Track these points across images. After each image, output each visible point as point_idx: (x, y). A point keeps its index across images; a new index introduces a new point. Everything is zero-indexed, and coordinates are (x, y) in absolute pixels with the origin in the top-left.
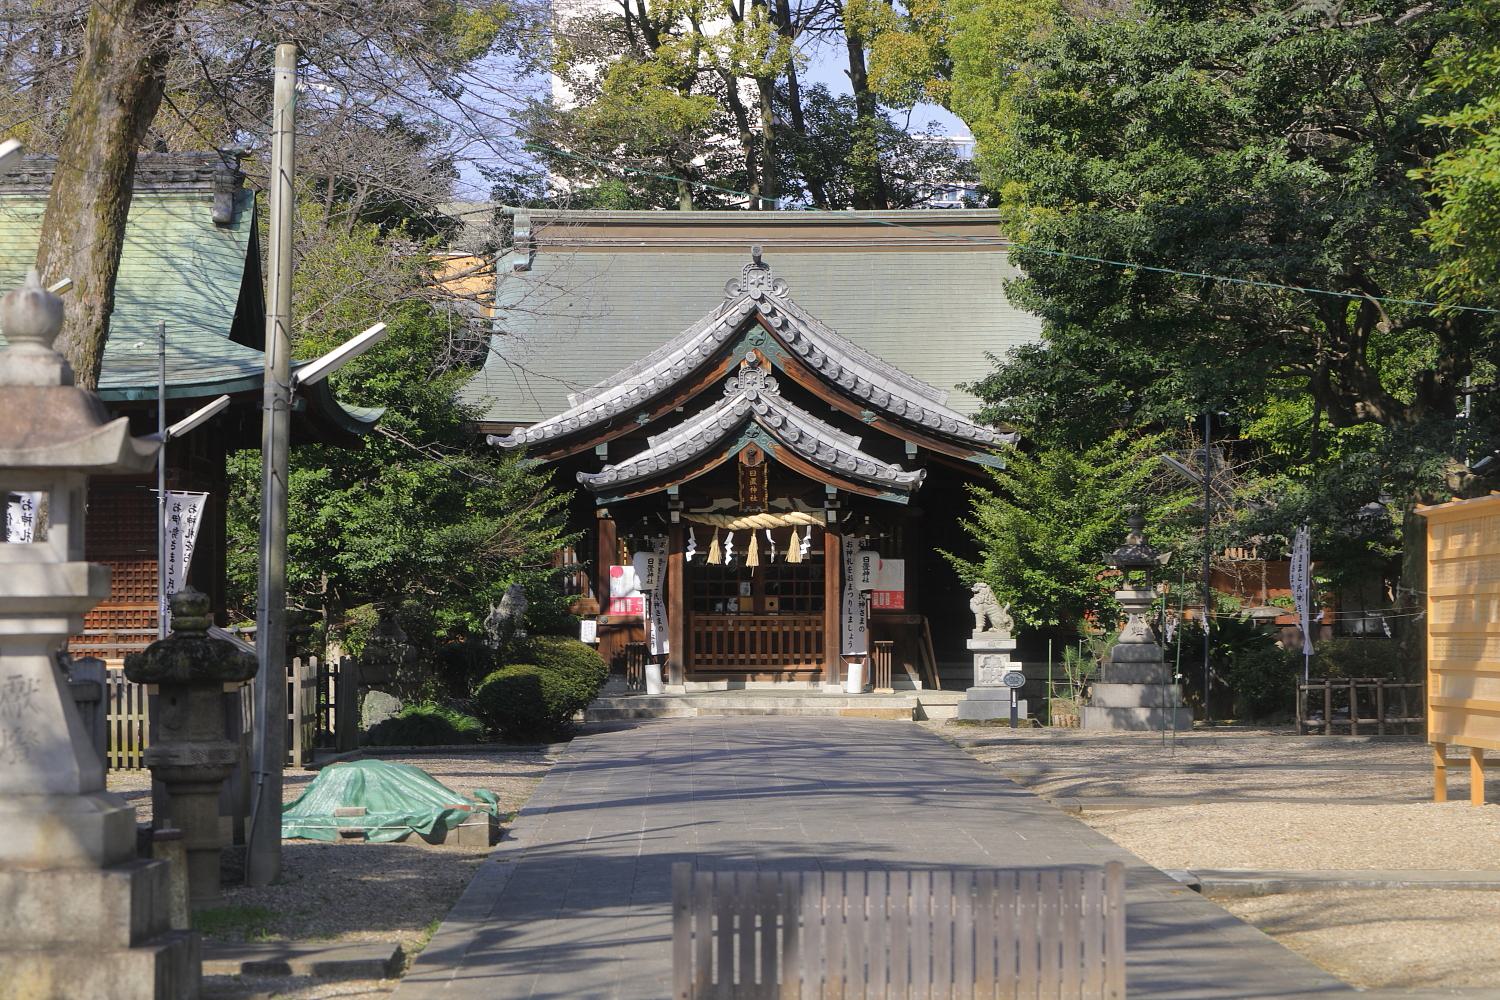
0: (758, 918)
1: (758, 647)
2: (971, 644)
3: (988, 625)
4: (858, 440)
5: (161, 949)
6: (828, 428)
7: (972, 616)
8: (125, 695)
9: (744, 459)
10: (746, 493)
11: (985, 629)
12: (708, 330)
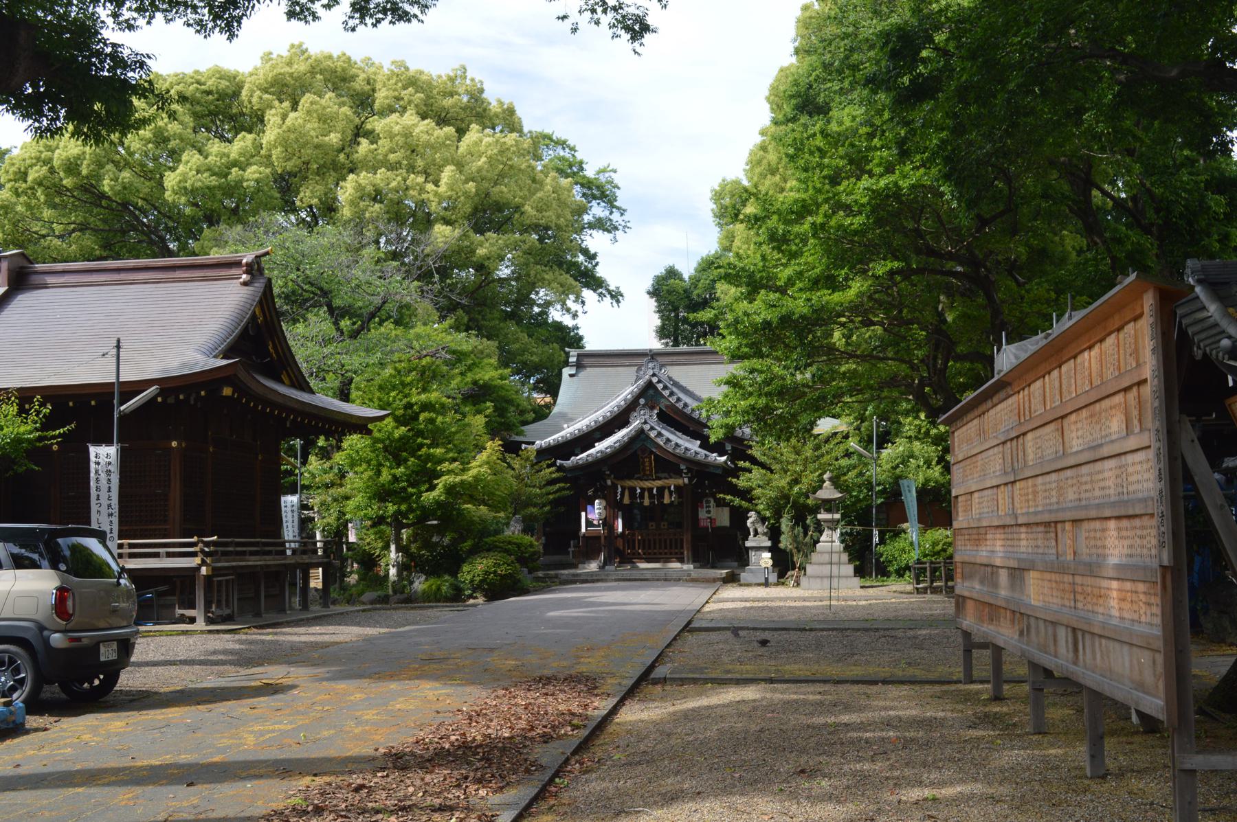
0: (1231, 384)
1: (658, 546)
2: (748, 544)
3: (756, 533)
4: (699, 442)
5: (858, 563)
6: (684, 436)
7: (748, 529)
8: (224, 588)
9: (639, 453)
10: (644, 470)
11: (755, 536)
12: (628, 391)
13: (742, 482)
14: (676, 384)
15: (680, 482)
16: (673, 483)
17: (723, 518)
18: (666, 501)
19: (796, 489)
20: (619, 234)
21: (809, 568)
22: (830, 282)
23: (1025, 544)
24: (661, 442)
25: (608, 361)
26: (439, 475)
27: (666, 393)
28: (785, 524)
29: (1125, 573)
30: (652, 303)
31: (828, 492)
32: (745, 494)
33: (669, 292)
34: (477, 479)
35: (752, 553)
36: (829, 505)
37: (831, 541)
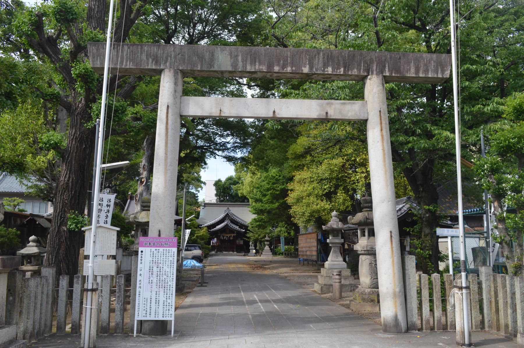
13: (248, 235)
14: (233, 214)
15: (234, 235)
16: (232, 235)
17: (242, 242)
18: (231, 239)
19: (260, 237)
20: (206, 169)
21: (263, 253)
22: (272, 202)
23: (307, 249)
24: (231, 227)
25: (211, 206)
26: (195, 233)
27: (231, 216)
28: (258, 244)
29: (315, 251)
30: (214, 188)
31: (267, 238)
32: (249, 238)
33: (219, 185)
34: (203, 234)
35: (251, 250)
36: (267, 241)
37: (267, 248)
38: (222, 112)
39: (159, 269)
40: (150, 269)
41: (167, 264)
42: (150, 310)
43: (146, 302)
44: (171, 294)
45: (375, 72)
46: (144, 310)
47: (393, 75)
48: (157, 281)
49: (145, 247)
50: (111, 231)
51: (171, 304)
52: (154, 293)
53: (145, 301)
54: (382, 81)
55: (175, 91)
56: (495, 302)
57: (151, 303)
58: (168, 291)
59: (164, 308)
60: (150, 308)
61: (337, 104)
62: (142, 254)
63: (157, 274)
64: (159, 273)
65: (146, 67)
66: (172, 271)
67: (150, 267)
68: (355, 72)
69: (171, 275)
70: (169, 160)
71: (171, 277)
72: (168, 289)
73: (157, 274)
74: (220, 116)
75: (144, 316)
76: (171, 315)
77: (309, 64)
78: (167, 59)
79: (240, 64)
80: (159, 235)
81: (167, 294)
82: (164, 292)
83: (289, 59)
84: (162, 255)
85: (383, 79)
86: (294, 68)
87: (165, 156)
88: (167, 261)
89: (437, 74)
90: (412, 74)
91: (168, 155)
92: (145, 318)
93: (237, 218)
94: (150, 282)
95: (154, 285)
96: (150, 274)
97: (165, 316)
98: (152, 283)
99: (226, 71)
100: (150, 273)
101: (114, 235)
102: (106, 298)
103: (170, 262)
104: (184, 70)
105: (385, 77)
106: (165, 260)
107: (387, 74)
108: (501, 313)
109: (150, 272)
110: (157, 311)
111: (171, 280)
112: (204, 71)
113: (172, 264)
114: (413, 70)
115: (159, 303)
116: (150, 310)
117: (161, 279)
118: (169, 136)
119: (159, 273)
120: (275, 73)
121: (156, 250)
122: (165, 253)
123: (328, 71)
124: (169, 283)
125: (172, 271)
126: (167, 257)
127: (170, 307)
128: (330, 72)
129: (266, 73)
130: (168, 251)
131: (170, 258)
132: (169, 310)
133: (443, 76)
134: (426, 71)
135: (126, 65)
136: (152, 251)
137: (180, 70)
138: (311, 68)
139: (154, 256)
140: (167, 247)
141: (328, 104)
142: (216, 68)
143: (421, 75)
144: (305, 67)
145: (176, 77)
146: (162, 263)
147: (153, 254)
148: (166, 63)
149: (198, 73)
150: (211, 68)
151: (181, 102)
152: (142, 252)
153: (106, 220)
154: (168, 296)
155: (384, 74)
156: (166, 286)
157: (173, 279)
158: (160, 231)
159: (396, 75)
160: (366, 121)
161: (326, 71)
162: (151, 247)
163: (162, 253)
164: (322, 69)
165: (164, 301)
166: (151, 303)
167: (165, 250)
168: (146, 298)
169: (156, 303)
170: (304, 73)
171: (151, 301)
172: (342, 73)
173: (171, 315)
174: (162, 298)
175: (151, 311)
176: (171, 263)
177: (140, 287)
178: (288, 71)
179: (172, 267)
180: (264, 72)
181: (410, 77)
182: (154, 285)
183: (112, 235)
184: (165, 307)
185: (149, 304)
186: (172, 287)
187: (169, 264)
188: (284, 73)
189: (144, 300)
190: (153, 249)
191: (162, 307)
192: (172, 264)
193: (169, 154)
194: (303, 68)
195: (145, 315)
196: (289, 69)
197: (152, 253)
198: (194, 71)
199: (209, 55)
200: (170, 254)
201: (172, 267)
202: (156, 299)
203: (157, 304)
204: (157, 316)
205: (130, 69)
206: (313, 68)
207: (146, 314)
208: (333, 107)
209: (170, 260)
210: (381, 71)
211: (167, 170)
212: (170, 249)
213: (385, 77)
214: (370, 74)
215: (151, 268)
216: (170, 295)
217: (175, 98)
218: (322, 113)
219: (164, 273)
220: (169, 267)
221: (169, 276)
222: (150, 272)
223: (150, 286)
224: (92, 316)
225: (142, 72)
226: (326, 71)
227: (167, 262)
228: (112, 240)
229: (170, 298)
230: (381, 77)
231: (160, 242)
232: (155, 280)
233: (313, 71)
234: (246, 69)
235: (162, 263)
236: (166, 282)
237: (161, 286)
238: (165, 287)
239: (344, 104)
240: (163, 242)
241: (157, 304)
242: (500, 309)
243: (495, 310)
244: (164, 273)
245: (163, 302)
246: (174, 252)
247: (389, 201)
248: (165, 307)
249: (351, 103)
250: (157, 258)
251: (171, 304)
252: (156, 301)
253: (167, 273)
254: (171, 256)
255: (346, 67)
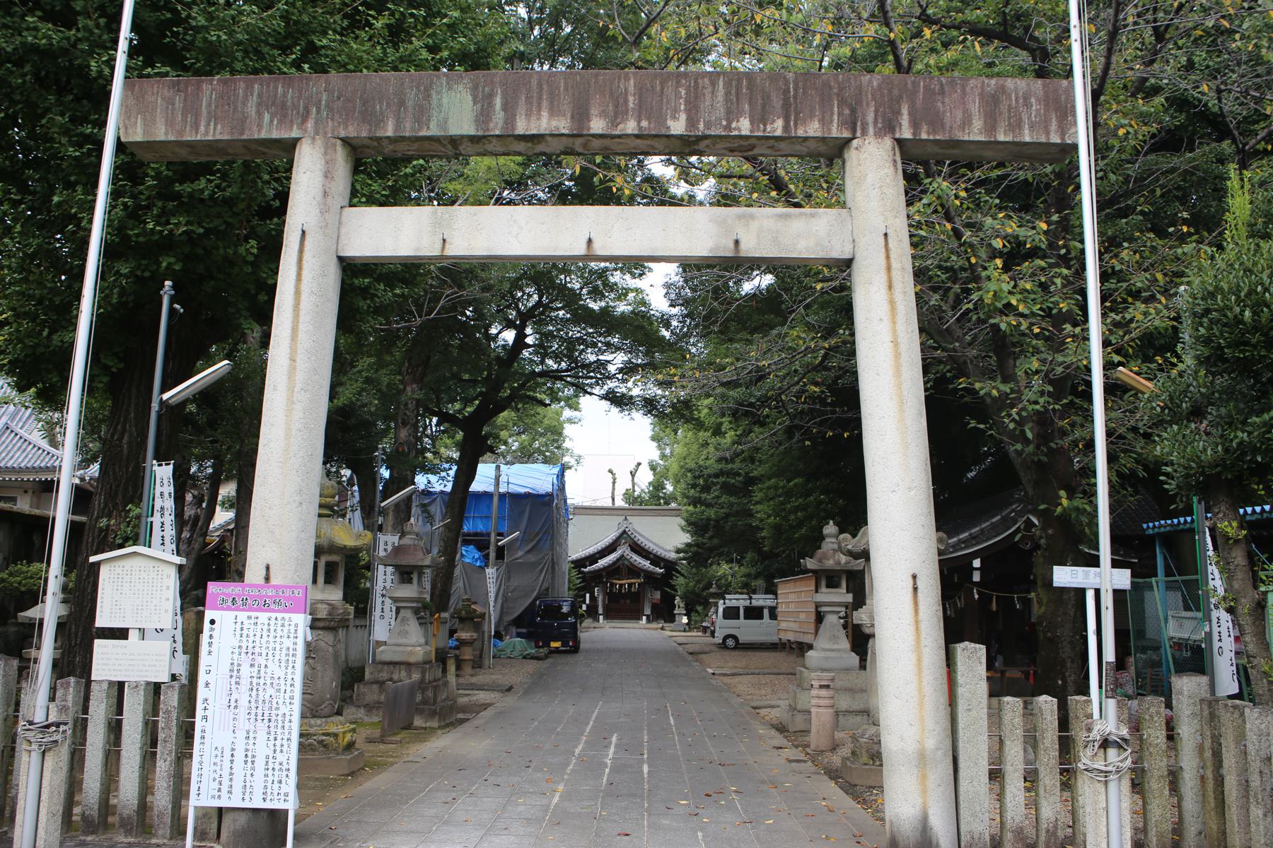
38: (447, 246)
39: (256, 669)
40: (231, 671)
41: (277, 657)
42: (231, 780)
43: (219, 758)
44: (285, 738)
45: (871, 130)
46: (214, 780)
47: (924, 136)
48: (250, 702)
49: (222, 609)
50: (163, 567)
51: (285, 766)
52: (241, 734)
53: (216, 756)
54: (891, 153)
55: (325, 194)
56: (1215, 779)
57: (232, 762)
58: (279, 731)
59: (266, 776)
60: (231, 774)
61: (768, 217)
62: (212, 630)
63: (251, 682)
64: (255, 681)
65: (256, 137)
66: (289, 677)
67: (232, 664)
68: (813, 129)
69: (289, 689)
70: (300, 377)
71: (288, 694)
72: (280, 724)
73: (251, 682)
74: (442, 257)
75: (213, 797)
76: (286, 795)
77: (688, 111)
78: (307, 111)
79: (499, 116)
80: (267, 579)
81: (275, 739)
82: (269, 733)
83: (631, 99)
84: (265, 634)
85: (894, 149)
86: (644, 124)
87: (291, 365)
88: (278, 649)
89: (1048, 134)
90: (976, 133)
91: (298, 361)
92: (217, 800)
93: (647, 543)
94: (233, 704)
95: (242, 711)
96: (233, 683)
97: (269, 798)
98: (236, 707)
99: (463, 137)
100: (233, 681)
101: (169, 577)
102: (133, 743)
103: (284, 651)
104: (350, 138)
105: (900, 142)
106: (272, 645)
107: (907, 134)
108: (1233, 813)
109: (231, 677)
110: (248, 784)
111: (288, 701)
112: (403, 139)
113: (291, 658)
114: (978, 123)
115: (253, 762)
116: (231, 780)
117: (261, 698)
118: (302, 313)
119: (255, 681)
120: (594, 136)
121: (249, 618)
122: (272, 628)
123: (739, 130)
124: (283, 709)
125: (289, 677)
126: (278, 639)
127: (285, 773)
128: (745, 132)
129: (571, 140)
130: (280, 622)
131: (285, 640)
132: (280, 782)
133: (1063, 139)
134: (1016, 126)
135: (207, 133)
136: (239, 621)
137: (342, 139)
138: (691, 122)
139: (244, 636)
140: (278, 611)
141: (740, 217)
142: (433, 130)
143: (1001, 137)
144: (674, 118)
145: (328, 157)
146: (264, 654)
147: (242, 629)
148: (304, 120)
149: (391, 147)
150: (420, 129)
151: (340, 223)
152: (212, 622)
153: (162, 533)
154: (278, 743)
155: (897, 136)
156: (273, 718)
157: (292, 698)
158: (268, 568)
159: (931, 137)
160: (848, 263)
161: (735, 129)
162: (238, 609)
163: (266, 627)
164: (724, 123)
165: (267, 757)
166: (232, 762)
167: (273, 619)
168: (219, 749)
169: (246, 762)
170: (672, 135)
171: (232, 755)
172: (779, 133)
173: (286, 795)
174: (262, 749)
175: (233, 783)
176: (287, 655)
177: (205, 718)
178: (630, 132)
179: (291, 665)
180: (563, 135)
181: (969, 141)
182: (242, 711)
183: (165, 577)
184: (270, 772)
185: (227, 764)
186: (290, 721)
187: (284, 658)
188: (619, 136)
189: (214, 753)
190: (242, 616)
191: (264, 772)
192: (291, 658)
193: (301, 358)
194: (670, 123)
195: (217, 794)
196: (630, 127)
197: (239, 625)
198: (379, 139)
199: (417, 95)
200: (286, 629)
201: (291, 665)
202: (247, 750)
203: (249, 764)
204: (247, 797)
205: (217, 141)
206: (698, 121)
207: (219, 790)
208: (754, 225)
209: (285, 646)
210: (889, 127)
211: (293, 403)
212: (287, 616)
213: (900, 142)
214: (858, 134)
215: (235, 668)
216: (285, 742)
217: (325, 210)
218: (724, 241)
219: (268, 682)
220: (283, 664)
221: (282, 691)
222: (231, 677)
223: (232, 717)
224: (43, 798)
225: (249, 149)
226: (735, 129)
227: (277, 652)
228: (164, 588)
229: (285, 749)
230: (888, 142)
231: (261, 597)
232: (244, 701)
233: (698, 129)
234: (513, 128)
235: (264, 654)
236: (275, 705)
237: (260, 718)
238: (270, 720)
239: (787, 216)
240: (268, 597)
241: (249, 764)
242: (1227, 802)
243: (1213, 805)
244: (268, 682)
245: (264, 760)
246: (296, 625)
247: (910, 489)
248: (270, 772)
249: (806, 215)
250: (251, 639)
251: (285, 766)
252: (246, 756)
253: (276, 682)
254: (289, 637)
255: (790, 112)
